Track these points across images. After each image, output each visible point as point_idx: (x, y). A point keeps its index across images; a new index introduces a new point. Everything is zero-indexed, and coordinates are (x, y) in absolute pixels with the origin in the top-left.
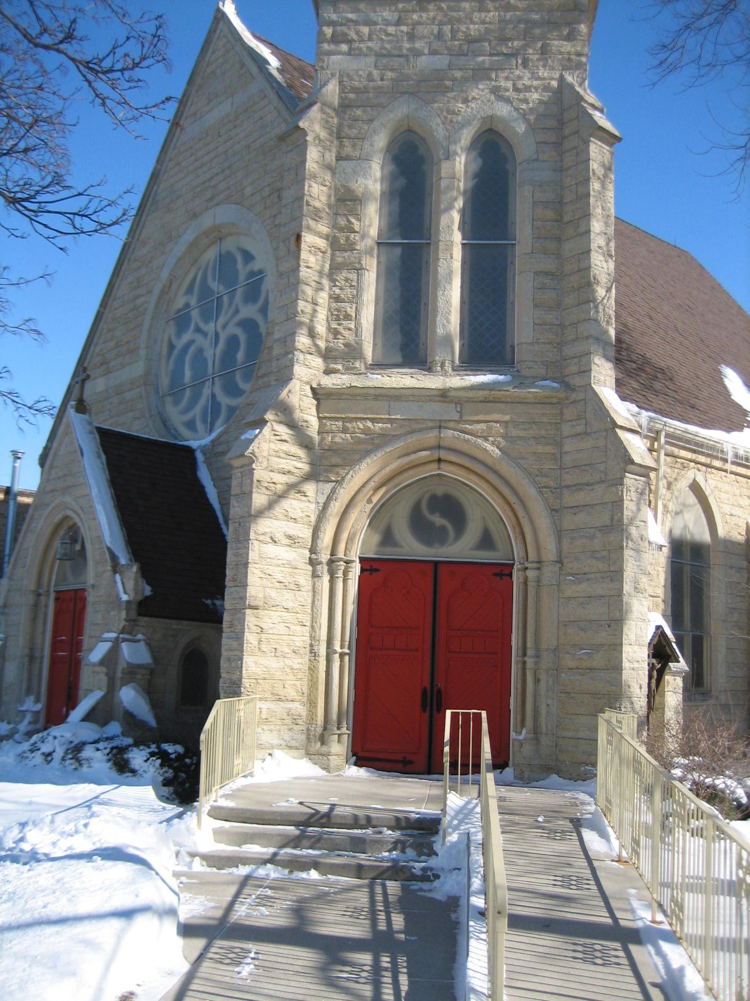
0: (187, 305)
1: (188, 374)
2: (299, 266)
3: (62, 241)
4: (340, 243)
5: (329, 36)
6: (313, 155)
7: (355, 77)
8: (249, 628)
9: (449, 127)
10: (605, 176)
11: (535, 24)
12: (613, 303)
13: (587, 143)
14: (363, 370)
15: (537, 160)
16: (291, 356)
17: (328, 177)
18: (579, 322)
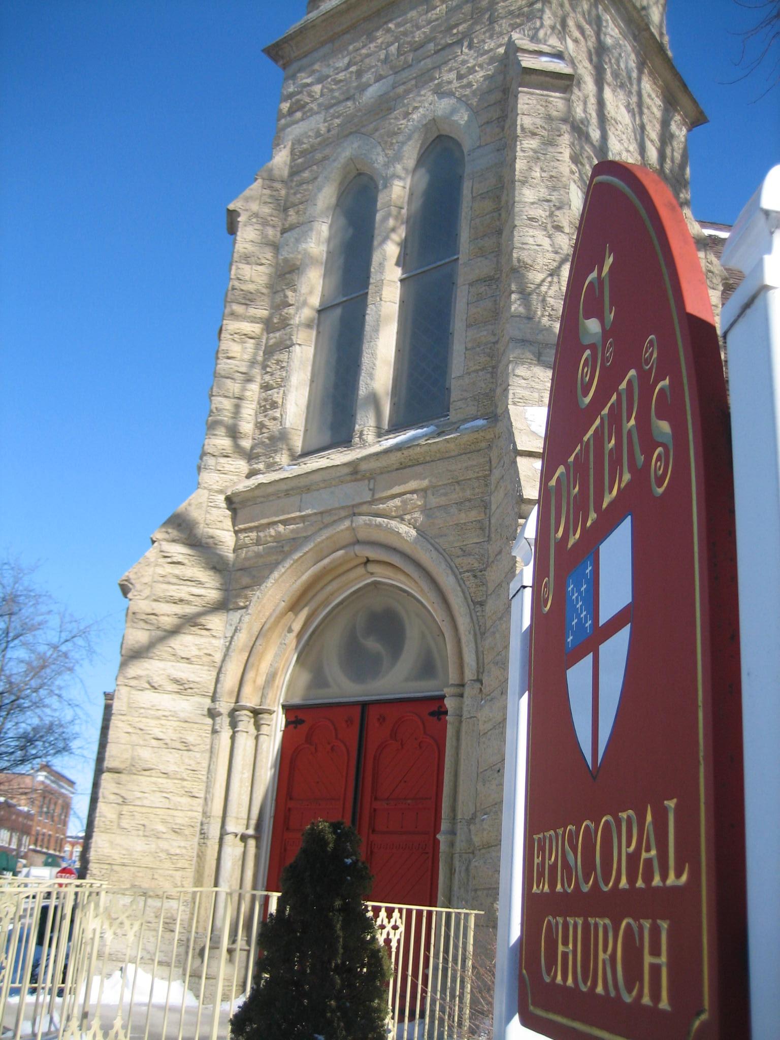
4: (277, 325)
8: (104, 797)
17: (269, 254)
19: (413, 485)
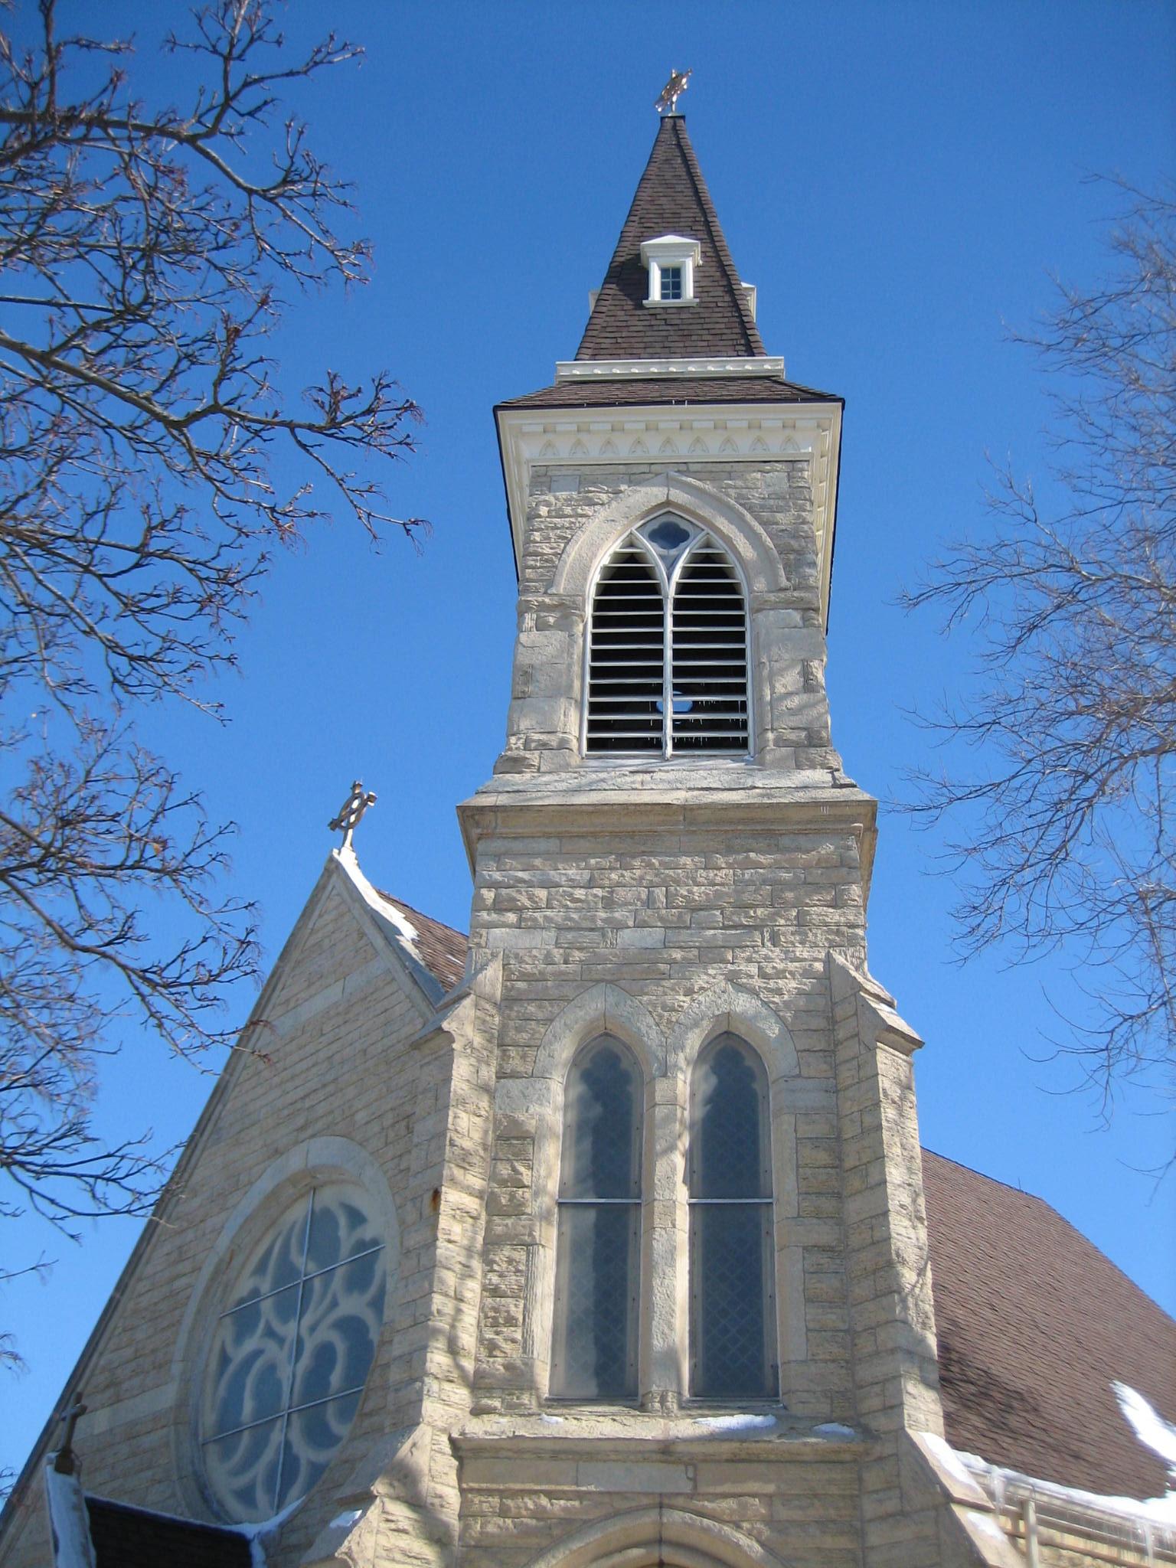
0: (255, 1293)
1: (248, 1406)
2: (436, 1239)
3: (74, 1224)
4: (502, 1205)
5: (489, 902)
6: (462, 1070)
7: (526, 959)
9: (665, 1029)
10: (903, 1098)
11: (778, 885)
12: (930, 1293)
13: (872, 1051)
14: (535, 1409)
15: (799, 1076)
16: (418, 1384)
17: (484, 1103)
18: (879, 1325)
19: (754, 1487)
